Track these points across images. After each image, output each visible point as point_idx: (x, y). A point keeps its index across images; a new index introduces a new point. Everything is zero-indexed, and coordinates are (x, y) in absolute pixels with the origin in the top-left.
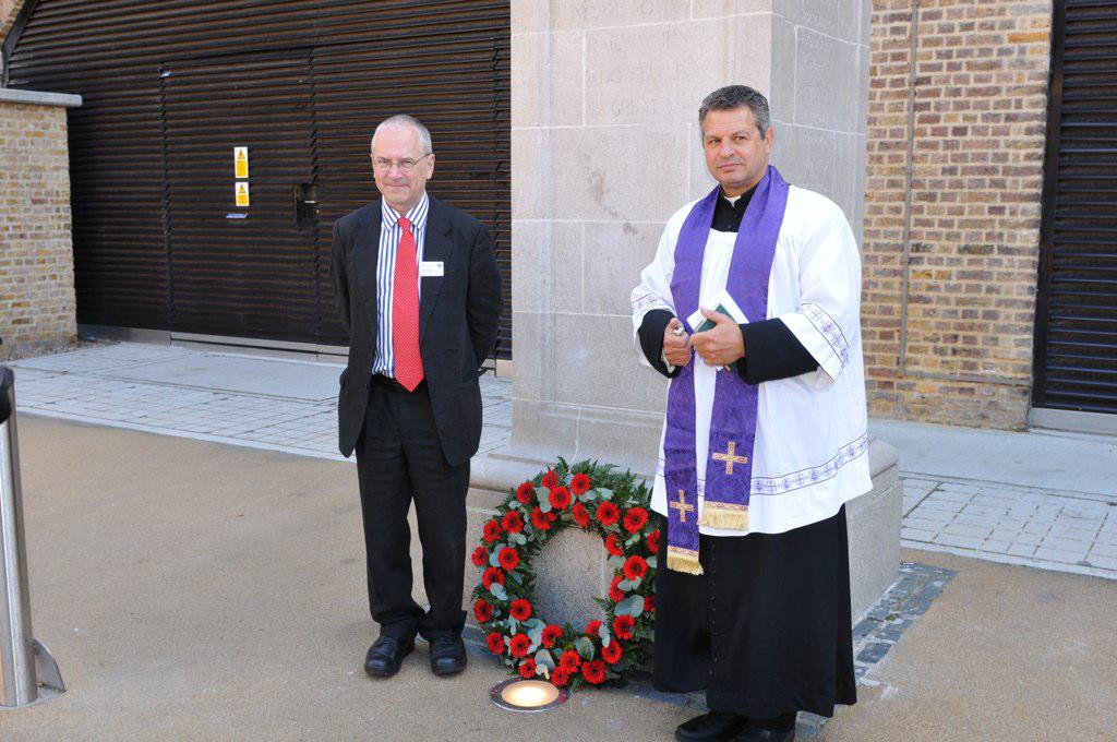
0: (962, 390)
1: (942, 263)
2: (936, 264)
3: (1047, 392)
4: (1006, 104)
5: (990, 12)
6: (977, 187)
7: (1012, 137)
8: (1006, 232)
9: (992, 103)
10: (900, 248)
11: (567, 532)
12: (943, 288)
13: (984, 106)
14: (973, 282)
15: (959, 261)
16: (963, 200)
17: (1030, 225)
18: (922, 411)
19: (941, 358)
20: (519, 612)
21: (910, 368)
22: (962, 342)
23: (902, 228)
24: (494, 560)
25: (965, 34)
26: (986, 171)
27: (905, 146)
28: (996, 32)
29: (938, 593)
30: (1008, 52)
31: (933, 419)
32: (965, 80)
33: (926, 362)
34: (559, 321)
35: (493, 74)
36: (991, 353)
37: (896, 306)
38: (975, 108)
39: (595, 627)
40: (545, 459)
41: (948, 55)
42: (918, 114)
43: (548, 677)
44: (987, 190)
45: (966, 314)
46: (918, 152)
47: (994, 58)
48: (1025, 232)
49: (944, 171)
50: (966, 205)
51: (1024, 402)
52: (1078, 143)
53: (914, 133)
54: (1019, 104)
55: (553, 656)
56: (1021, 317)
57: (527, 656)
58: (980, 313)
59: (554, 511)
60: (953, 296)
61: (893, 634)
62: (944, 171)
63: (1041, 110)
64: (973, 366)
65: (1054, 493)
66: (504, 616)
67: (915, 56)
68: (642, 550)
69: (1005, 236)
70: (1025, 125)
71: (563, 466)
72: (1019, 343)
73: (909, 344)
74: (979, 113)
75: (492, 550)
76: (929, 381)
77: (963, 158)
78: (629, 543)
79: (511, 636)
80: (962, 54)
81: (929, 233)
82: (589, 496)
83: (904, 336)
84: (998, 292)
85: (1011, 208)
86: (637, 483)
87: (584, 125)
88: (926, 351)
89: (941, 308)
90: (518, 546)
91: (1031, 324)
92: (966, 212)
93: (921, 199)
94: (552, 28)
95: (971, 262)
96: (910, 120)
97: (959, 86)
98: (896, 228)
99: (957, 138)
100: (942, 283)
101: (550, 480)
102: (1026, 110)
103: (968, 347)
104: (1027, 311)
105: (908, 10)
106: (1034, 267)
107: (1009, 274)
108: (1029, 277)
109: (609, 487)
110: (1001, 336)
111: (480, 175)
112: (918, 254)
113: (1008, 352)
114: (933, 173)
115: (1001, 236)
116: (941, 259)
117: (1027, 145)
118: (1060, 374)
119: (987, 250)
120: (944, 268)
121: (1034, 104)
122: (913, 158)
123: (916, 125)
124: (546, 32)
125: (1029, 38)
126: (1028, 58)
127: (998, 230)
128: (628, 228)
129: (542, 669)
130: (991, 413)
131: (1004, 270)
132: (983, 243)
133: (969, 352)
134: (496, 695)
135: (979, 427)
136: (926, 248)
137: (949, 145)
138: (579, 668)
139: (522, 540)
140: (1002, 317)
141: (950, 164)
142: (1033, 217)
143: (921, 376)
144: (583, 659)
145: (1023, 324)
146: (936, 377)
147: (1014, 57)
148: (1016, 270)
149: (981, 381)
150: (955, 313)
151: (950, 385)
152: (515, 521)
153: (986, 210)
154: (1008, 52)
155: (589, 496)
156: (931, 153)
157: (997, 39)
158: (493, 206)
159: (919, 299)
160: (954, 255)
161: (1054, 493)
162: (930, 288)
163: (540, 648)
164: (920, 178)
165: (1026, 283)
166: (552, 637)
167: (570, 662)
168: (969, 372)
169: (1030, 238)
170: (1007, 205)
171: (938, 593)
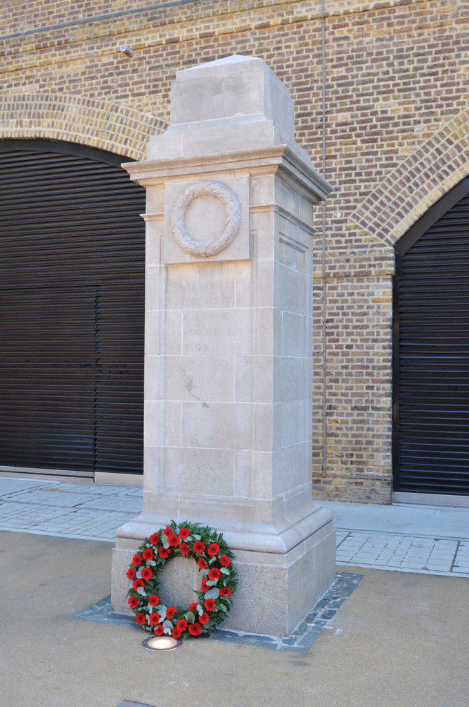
0: (356, 483)
1: (343, 416)
2: (340, 416)
3: (401, 483)
4: (372, 333)
5: (362, 287)
6: (359, 376)
7: (376, 350)
8: (375, 399)
9: (365, 333)
10: (322, 408)
11: (175, 559)
12: (344, 428)
13: (361, 334)
14: (359, 425)
15: (352, 414)
16: (353, 382)
17: (387, 395)
18: (337, 495)
19: (344, 466)
20: (153, 601)
21: (329, 472)
22: (355, 458)
23: (322, 397)
24: (139, 575)
25: (349, 298)
26: (364, 367)
27: (322, 354)
28: (365, 297)
29: (356, 586)
30: (372, 307)
31: (342, 499)
32: (351, 321)
33: (337, 469)
34: (168, 451)
35: (96, 310)
36: (371, 463)
37: (320, 438)
38: (356, 335)
39: (193, 608)
40: (163, 522)
41: (342, 308)
42: (328, 338)
43: (170, 634)
44: (365, 377)
45: (358, 442)
46: (329, 357)
47: (365, 310)
48: (385, 399)
49: (342, 367)
50: (354, 385)
51: (389, 489)
52: (408, 354)
53: (326, 347)
54: (378, 334)
55: (173, 623)
56: (385, 443)
57: (158, 624)
58: (364, 442)
59: (170, 547)
60: (350, 433)
61: (337, 605)
62: (342, 367)
63: (389, 337)
64: (362, 470)
65: (407, 535)
66: (145, 603)
67: (325, 308)
68: (218, 565)
69: (375, 401)
70: (382, 344)
71: (174, 524)
72: (386, 457)
73: (328, 459)
74: (358, 338)
75: (137, 569)
76: (339, 480)
77: (352, 360)
78: (211, 562)
79: (149, 615)
80: (349, 308)
81: (336, 400)
82: (189, 539)
83: (325, 454)
84: (373, 431)
85: (377, 386)
86: (212, 532)
87: (182, 355)
88: (337, 462)
89: (344, 439)
90: (151, 567)
91: (390, 447)
92: (355, 388)
93: (331, 382)
94: (166, 308)
95: (358, 415)
96: (324, 341)
97: (348, 324)
98: (319, 397)
99: (348, 350)
100: (344, 426)
101: (168, 532)
102: (382, 337)
103: (358, 460)
104: (387, 440)
105: (321, 285)
106: (390, 417)
107: (377, 421)
108: (388, 422)
109: (199, 534)
110: (375, 454)
111: (86, 366)
112: (331, 411)
113: (379, 462)
114: (337, 368)
115: (373, 401)
116: (343, 413)
117: (383, 354)
118: (406, 473)
119: (366, 408)
120: (344, 418)
121: (386, 334)
122: (326, 360)
123: (327, 344)
124: (163, 310)
125: (382, 301)
126: (382, 310)
127: (371, 398)
128: (204, 405)
129: (167, 630)
130: (372, 495)
131: (375, 419)
132: (364, 405)
133: (359, 463)
134: (145, 644)
135: (366, 503)
136: (335, 408)
137: (344, 354)
138: (187, 628)
139: (154, 564)
140: (375, 443)
141: (345, 364)
142: (388, 391)
143: (335, 476)
144: (188, 624)
145: (386, 447)
146: (343, 477)
147: (375, 310)
148: (381, 419)
149: (366, 478)
150: (351, 442)
151: (350, 481)
152: (149, 554)
153: (365, 388)
154: (372, 307)
155: (189, 539)
156: (335, 358)
157: (366, 301)
158: (94, 383)
159: (332, 435)
160: (349, 411)
161: (407, 535)
162: (338, 429)
163: (165, 619)
164: (330, 371)
165: (386, 426)
166: (171, 613)
167: (182, 625)
168: (360, 473)
169: (387, 402)
170: (375, 385)
171: (356, 586)
